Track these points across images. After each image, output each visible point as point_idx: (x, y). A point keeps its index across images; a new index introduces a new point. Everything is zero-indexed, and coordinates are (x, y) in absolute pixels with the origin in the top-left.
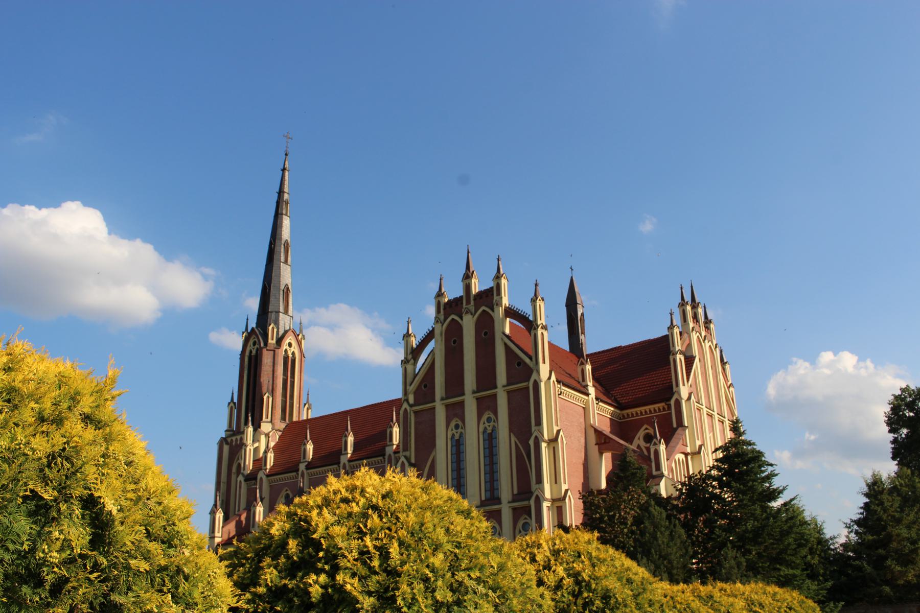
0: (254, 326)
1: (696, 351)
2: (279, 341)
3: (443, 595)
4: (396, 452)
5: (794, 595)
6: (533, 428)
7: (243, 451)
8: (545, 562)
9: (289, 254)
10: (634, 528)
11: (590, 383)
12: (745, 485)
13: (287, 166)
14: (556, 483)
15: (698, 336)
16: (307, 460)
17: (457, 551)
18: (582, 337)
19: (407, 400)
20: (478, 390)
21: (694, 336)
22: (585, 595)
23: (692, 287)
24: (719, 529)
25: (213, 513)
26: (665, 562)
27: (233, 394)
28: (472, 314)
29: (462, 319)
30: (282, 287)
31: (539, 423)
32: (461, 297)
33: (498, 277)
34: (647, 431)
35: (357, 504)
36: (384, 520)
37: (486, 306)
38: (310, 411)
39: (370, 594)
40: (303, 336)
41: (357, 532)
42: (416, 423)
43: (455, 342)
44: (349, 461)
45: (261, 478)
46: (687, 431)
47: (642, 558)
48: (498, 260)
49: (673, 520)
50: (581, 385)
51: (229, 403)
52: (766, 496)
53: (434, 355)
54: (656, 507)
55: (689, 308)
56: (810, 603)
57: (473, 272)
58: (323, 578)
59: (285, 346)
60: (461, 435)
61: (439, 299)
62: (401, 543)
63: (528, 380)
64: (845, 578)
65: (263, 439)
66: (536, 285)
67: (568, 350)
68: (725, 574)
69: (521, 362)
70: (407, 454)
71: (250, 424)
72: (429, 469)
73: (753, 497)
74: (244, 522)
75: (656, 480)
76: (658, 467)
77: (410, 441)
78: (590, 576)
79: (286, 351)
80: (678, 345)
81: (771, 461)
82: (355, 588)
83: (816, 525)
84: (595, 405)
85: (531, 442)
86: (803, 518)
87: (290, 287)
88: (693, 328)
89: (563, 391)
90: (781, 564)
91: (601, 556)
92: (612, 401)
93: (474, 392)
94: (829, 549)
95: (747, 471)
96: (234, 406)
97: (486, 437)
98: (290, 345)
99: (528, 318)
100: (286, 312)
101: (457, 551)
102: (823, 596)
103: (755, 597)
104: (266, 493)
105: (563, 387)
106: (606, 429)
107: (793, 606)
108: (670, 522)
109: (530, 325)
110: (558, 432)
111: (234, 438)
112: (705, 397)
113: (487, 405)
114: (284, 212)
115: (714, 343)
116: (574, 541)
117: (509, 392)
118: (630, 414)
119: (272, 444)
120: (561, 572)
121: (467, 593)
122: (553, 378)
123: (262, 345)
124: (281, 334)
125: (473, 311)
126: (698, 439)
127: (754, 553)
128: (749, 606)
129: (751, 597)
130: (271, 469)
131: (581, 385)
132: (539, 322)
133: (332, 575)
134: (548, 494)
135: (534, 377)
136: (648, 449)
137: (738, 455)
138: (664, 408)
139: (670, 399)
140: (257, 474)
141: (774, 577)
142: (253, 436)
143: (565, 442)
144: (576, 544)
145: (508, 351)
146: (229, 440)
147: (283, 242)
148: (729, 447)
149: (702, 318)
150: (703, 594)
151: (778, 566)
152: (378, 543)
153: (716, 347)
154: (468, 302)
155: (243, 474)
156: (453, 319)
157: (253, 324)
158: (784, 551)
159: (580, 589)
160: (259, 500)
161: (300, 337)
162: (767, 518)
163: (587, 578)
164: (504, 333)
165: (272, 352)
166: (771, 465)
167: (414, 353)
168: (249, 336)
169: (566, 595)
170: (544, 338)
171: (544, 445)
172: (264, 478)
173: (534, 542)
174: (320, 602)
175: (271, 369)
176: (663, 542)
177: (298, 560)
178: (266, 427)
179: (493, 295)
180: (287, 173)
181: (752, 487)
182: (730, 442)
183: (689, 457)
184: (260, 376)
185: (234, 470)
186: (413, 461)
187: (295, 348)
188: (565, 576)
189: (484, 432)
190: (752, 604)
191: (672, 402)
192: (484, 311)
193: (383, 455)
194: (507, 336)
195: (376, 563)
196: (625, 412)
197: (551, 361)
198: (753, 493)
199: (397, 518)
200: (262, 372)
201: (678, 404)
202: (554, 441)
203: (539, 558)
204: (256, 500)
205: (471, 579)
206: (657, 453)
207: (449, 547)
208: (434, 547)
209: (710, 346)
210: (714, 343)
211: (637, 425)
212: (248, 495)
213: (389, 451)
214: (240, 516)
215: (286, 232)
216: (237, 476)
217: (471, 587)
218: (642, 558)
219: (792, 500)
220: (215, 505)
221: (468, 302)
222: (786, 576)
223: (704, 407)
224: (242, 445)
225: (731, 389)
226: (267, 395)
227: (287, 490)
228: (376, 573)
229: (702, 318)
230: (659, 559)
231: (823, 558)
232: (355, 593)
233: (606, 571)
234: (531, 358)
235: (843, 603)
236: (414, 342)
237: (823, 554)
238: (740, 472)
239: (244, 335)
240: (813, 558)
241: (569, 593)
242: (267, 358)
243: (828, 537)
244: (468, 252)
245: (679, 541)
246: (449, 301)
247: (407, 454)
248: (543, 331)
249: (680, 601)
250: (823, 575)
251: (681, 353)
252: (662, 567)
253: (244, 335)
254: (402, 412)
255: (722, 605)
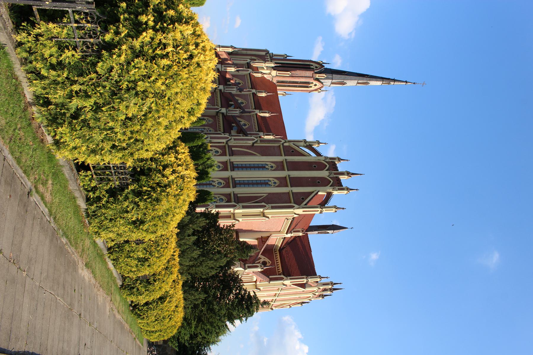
0: (325, 67)
1: (307, 289)
2: (317, 80)
3: (141, 86)
4: (260, 137)
5: (179, 323)
6: (270, 205)
7: (262, 62)
8: (177, 171)
9: (362, 85)
10: (216, 251)
11: (293, 235)
12: (236, 306)
13: (408, 83)
14: (242, 216)
15: (315, 291)
16: (257, 93)
17: (167, 98)
18: (316, 232)
19: (285, 142)
20: (290, 178)
21: (316, 289)
22: (159, 189)
23: (341, 289)
24: (214, 292)
25: (232, 47)
26: (199, 264)
27: (291, 56)
28: (329, 175)
29: (326, 170)
30: (345, 81)
31: (273, 208)
32: (338, 170)
33: (348, 189)
34: (268, 263)
35: (194, 49)
36: (184, 61)
37: (333, 183)
38: (282, 95)
39: (142, 47)
40: (320, 92)
41: (177, 45)
42: (274, 146)
43: (315, 166)
44: (256, 114)
45: (248, 71)
46: (268, 283)
47: (200, 252)
48: (356, 190)
49: (219, 269)
50: (292, 230)
51: (286, 55)
52: (231, 316)
53: (308, 156)
54: (226, 261)
55: (330, 287)
56: (175, 331)
57: (351, 177)
58: (151, 23)
59: (315, 82)
60: (268, 169)
61: (337, 159)
62: (170, 67)
63: (294, 203)
64: (190, 353)
65: (268, 72)
66: (343, 208)
67: (310, 225)
68: (192, 293)
69: (304, 200)
70: (259, 142)
71: (276, 65)
72: (251, 153)
73: (230, 309)
74: (227, 62)
75: (243, 266)
76: (249, 267)
77: (265, 143)
78: (168, 193)
79: (312, 83)
80: (311, 280)
81: (248, 320)
82: (144, 38)
83: (217, 342)
84: (281, 237)
85: (263, 204)
86: (220, 335)
87: (345, 85)
88: (320, 288)
89: (289, 220)
90: (197, 321)
91: (180, 200)
92: (283, 246)
93: (289, 176)
94: (205, 347)
95: (243, 307)
96: (285, 57)
97: (266, 181)
98: (315, 85)
99: (326, 204)
100: (332, 83)
101: (167, 98)
102: (181, 341)
103: (174, 299)
104: (241, 73)
105: (291, 220)
106: (270, 242)
107: (171, 320)
108: (218, 267)
109: (323, 204)
110: (268, 218)
111: (269, 57)
112: (285, 293)
113: (283, 182)
114: (384, 82)
115: (312, 299)
116: (189, 188)
117: (289, 193)
118: (277, 255)
119: (265, 76)
120: (171, 178)
121: (142, 99)
122: (296, 216)
123: (315, 71)
124: (321, 80)
125: (331, 176)
126: (263, 288)
127: (203, 308)
128: (170, 295)
129: (174, 297)
130: (253, 75)
131: (292, 230)
132: (324, 209)
133: (154, 28)
134: (237, 211)
135: (296, 206)
136: (259, 263)
137: (251, 303)
138: (279, 272)
139: (284, 275)
140: (250, 69)
141: (191, 318)
142: (270, 67)
143: (263, 221)
144: (187, 189)
145: (311, 193)
146: (268, 55)
147: (368, 82)
148: (256, 299)
149: (325, 293)
150: (173, 269)
151: (196, 320)
152: (170, 55)
153: (310, 300)
154: (335, 174)
155: (251, 62)
156: (326, 166)
157: (326, 66)
158: (203, 323)
159: (162, 186)
160: (238, 69)
161: (319, 90)
162: (219, 316)
163: (167, 190)
164: (318, 191)
165: (312, 76)
166: (246, 320)
167: (310, 146)
168: (321, 65)
169: (159, 179)
170: (316, 212)
171: (262, 210)
172: (249, 72)
173: (189, 168)
174: (139, 21)
175: (303, 76)
176: (208, 264)
177: (164, 15)
178: (274, 73)
179: (339, 186)
180: (404, 83)
181: (235, 309)
182: (258, 300)
183: (254, 283)
184: (300, 70)
185: (253, 57)
186: (255, 145)
187: (314, 88)
188: (169, 180)
189: (269, 180)
190: (170, 297)
191: (282, 276)
192: (331, 182)
193: (259, 131)
194: (317, 193)
195: (158, 52)
196: (278, 252)
197: (305, 215)
198: (232, 310)
199: (185, 68)
200: (302, 71)
201: (281, 279)
202: (264, 215)
203: (180, 168)
204: (237, 68)
205: (151, 104)
206: (257, 267)
207: (168, 95)
208: (169, 85)
209: (310, 297)
210: (312, 299)
211: (271, 257)
212: (240, 64)
213: (261, 134)
214: (230, 60)
215: (373, 83)
216: (249, 59)
217: (146, 102)
218: (200, 252)
219: (228, 329)
220: (236, 48)
221: (335, 174)
222: (191, 323)
223: (279, 292)
224: (265, 61)
225: (289, 307)
226: (290, 73)
227: (242, 83)
228: (154, 52)
229: (325, 293)
230: (200, 261)
231: (200, 343)
232: (141, 37)
233: (172, 202)
234: (305, 205)
235: (178, 350)
236: (315, 146)
237: (202, 343)
238: (243, 304)
239: (321, 62)
240: (200, 338)
241: (160, 181)
242: (309, 73)
243: (211, 346)
244: (361, 174)
245: (209, 271)
246: (336, 164)
247: (259, 142)
248: (319, 211)
249: (165, 251)
250: (192, 343)
251: (307, 282)
252: (196, 262)
253: (321, 62)
254: (280, 139)
255: (167, 278)
